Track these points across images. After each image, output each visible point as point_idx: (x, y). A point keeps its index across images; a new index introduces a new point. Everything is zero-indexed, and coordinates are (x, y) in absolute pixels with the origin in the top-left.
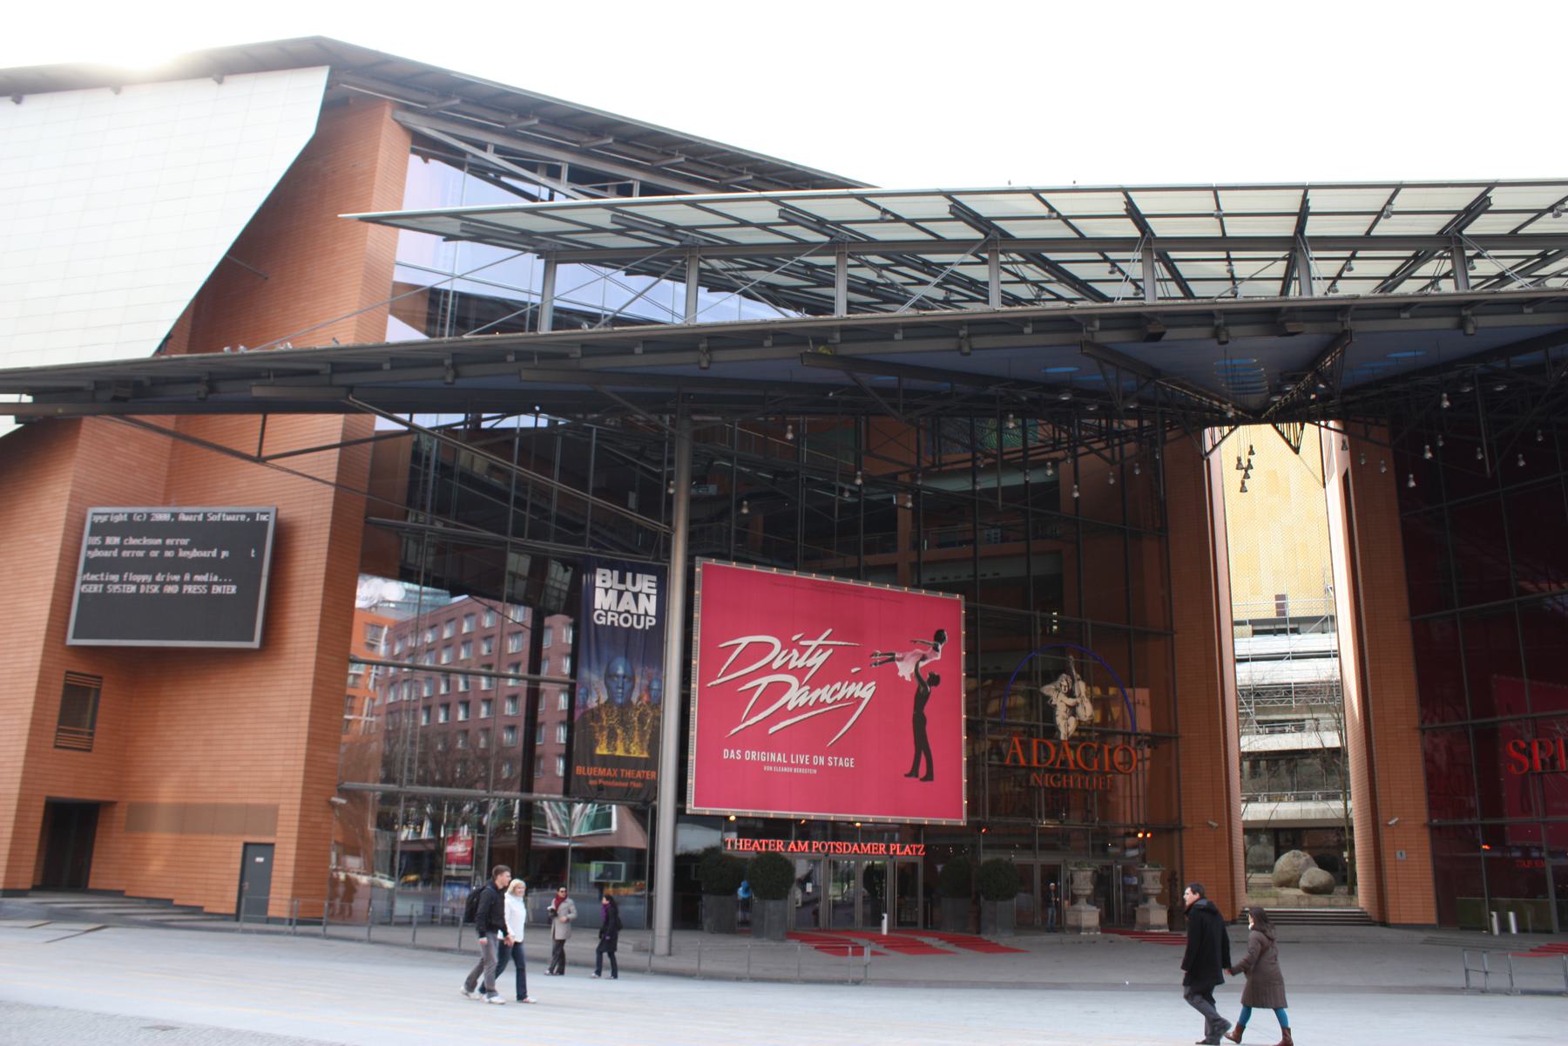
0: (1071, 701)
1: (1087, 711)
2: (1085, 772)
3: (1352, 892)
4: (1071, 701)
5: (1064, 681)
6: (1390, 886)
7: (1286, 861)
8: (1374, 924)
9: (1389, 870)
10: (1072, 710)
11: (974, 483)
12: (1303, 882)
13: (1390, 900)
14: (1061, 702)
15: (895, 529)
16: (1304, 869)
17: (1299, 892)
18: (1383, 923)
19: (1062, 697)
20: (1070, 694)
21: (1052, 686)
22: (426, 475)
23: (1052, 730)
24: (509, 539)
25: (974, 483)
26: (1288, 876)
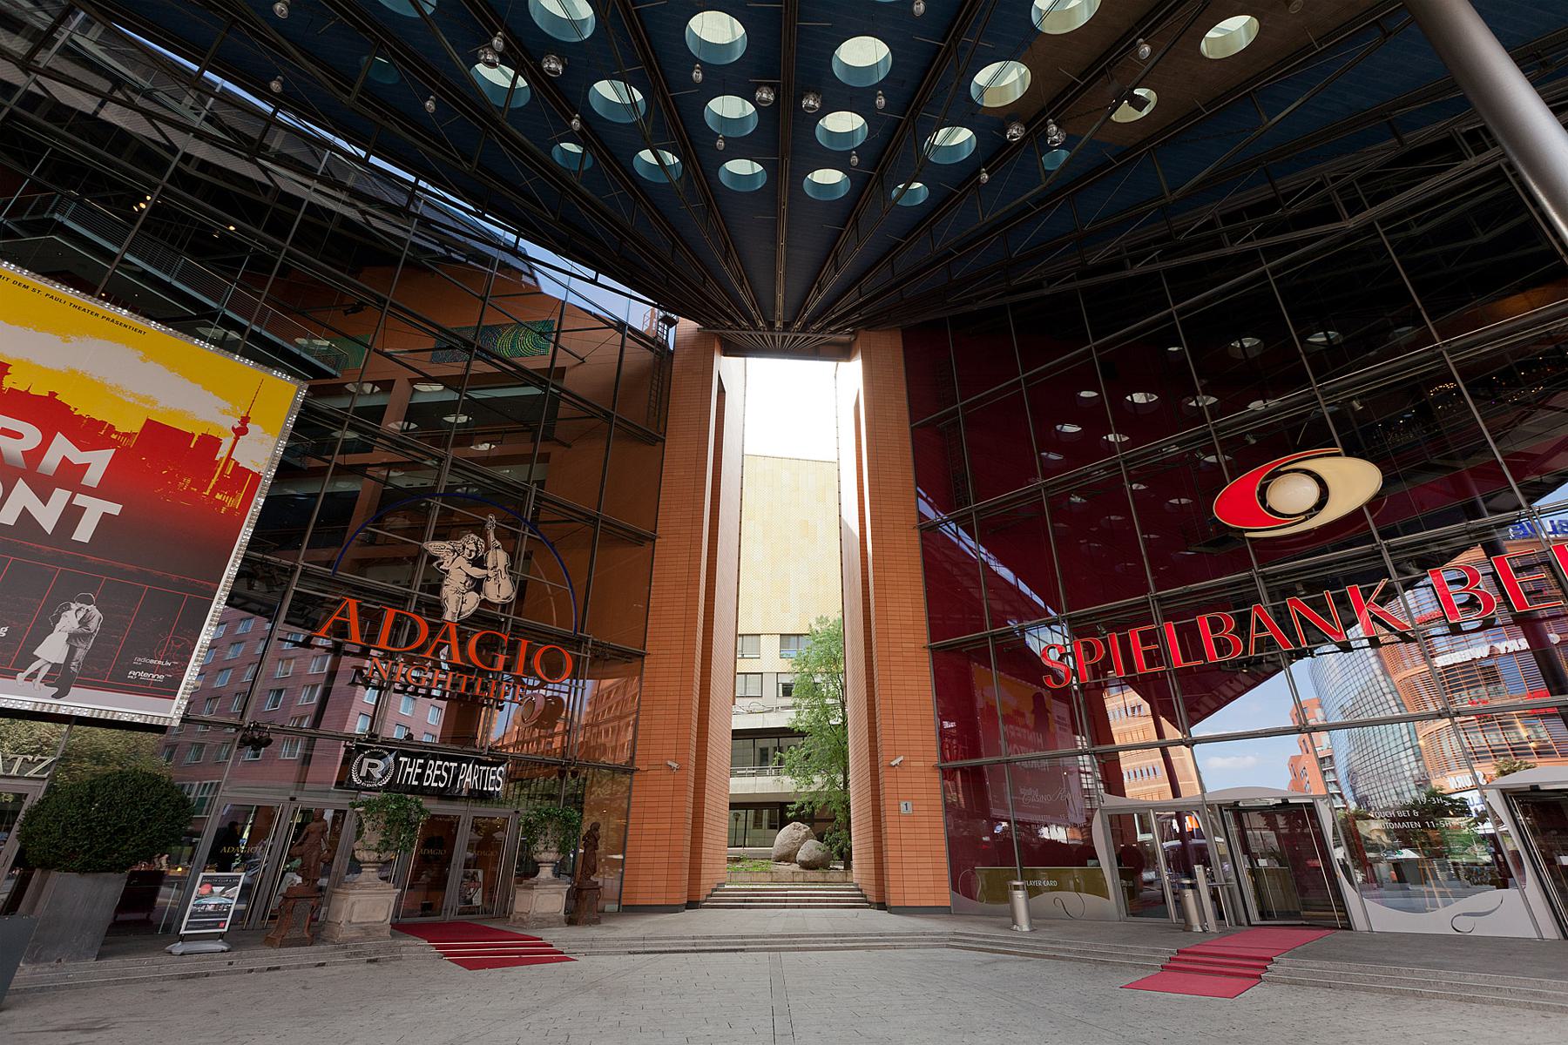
0: (477, 572)
1: (500, 590)
2: (482, 673)
3: (848, 866)
4: (477, 572)
5: (470, 542)
6: (891, 853)
7: (786, 836)
8: (871, 905)
9: (890, 829)
10: (478, 585)
11: (101, 105)
12: (801, 856)
13: (892, 871)
14: (456, 567)
15: (348, 523)
16: (802, 842)
17: (795, 867)
18: (882, 906)
19: (461, 561)
20: (479, 562)
21: (447, 545)
22: (187, 158)
23: (437, 609)
24: (1489, 519)
25: (101, 105)
26: (786, 850)
